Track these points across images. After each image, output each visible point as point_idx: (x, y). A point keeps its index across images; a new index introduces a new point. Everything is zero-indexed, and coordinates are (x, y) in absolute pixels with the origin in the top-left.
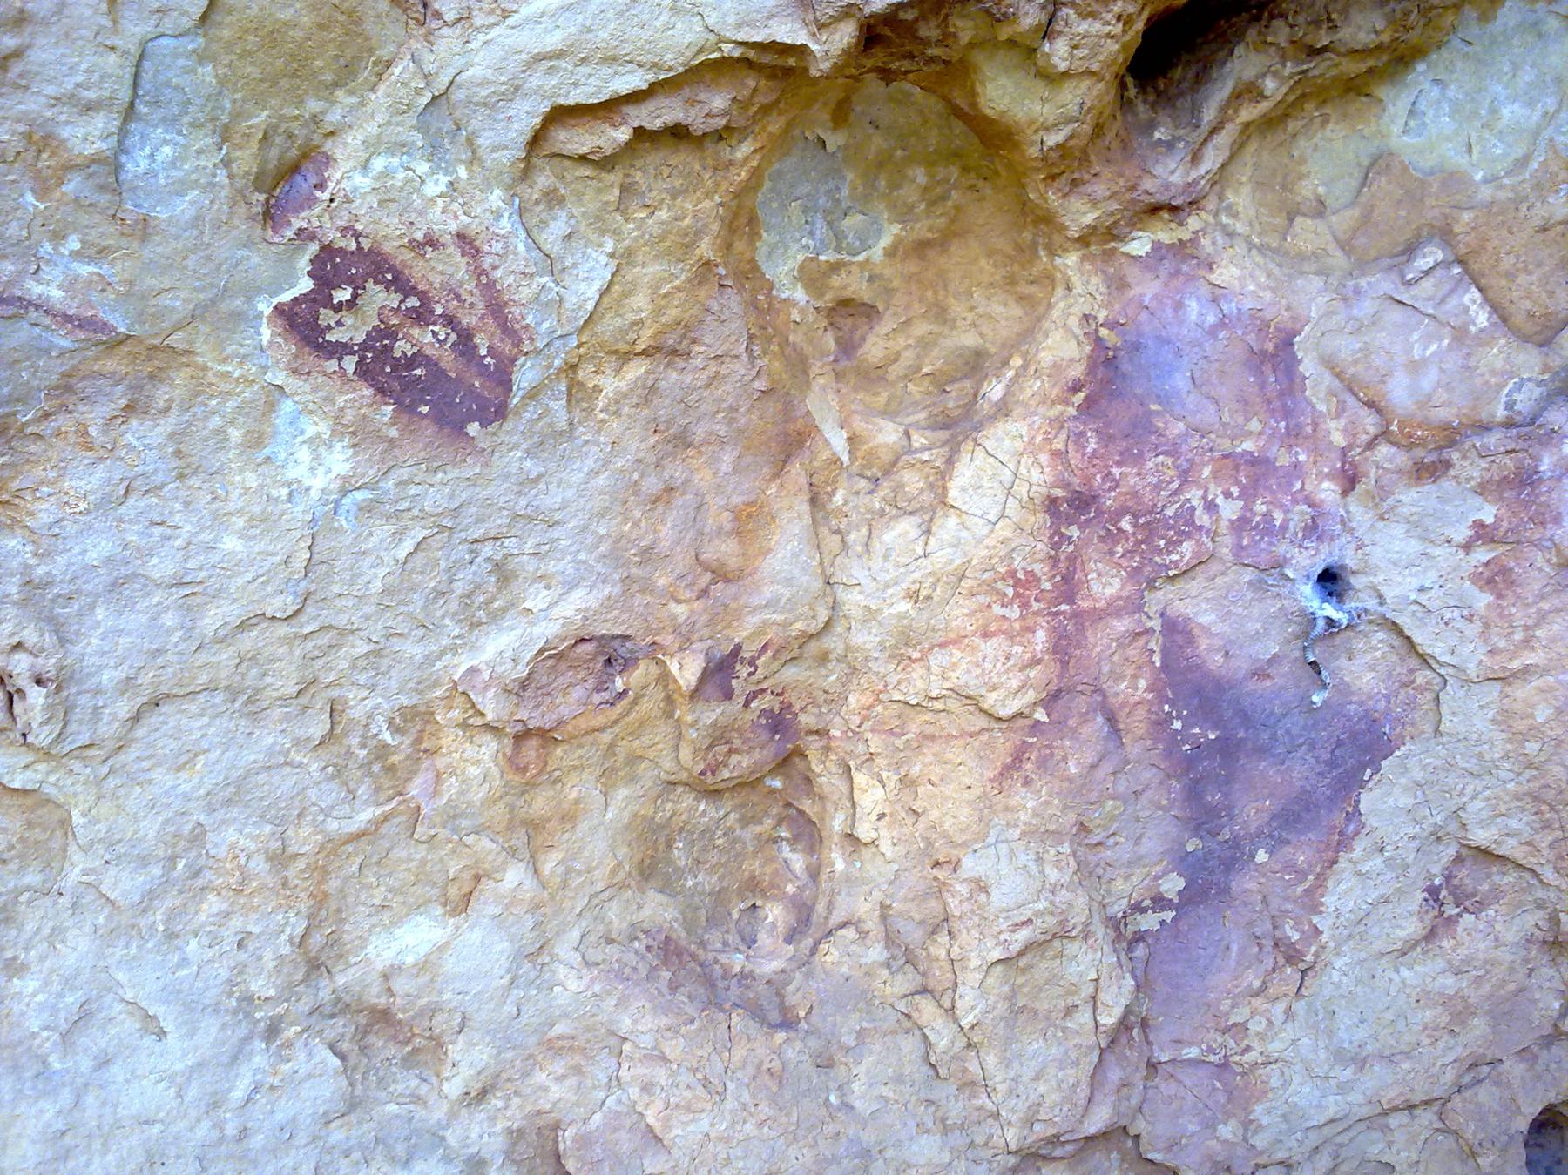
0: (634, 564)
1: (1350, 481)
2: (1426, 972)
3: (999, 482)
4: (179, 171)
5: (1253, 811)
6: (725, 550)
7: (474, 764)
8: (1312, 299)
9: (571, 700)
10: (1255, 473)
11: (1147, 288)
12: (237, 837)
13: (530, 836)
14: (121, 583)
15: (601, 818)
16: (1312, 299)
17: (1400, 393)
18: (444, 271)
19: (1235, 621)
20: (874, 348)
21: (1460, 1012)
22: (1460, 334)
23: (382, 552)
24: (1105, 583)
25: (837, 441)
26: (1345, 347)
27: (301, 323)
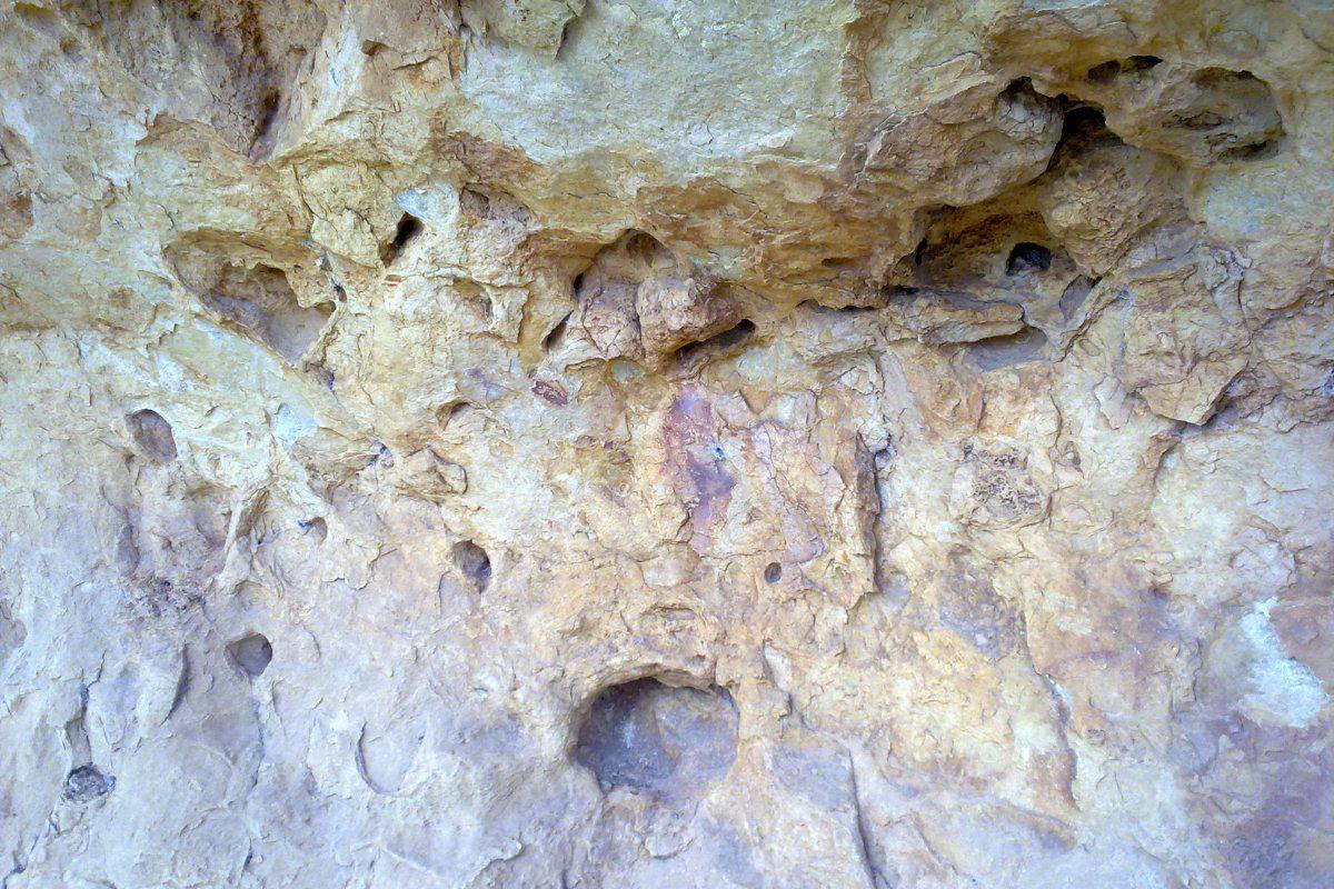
0: (594, 427)
1: (720, 434)
2: (747, 529)
3: (655, 422)
4: (517, 372)
5: (711, 490)
6: (610, 425)
7: (571, 453)
8: (714, 398)
9: (585, 445)
10: (702, 429)
11: (686, 390)
12: (535, 456)
13: (581, 465)
14: (516, 419)
15: (593, 466)
16: (714, 398)
17: (730, 418)
18: (554, 384)
19: (702, 454)
20: (643, 391)
21: (756, 540)
22: (742, 410)
23: (552, 421)
24: (675, 443)
25: (633, 409)
26: (720, 409)
27: (534, 390)
